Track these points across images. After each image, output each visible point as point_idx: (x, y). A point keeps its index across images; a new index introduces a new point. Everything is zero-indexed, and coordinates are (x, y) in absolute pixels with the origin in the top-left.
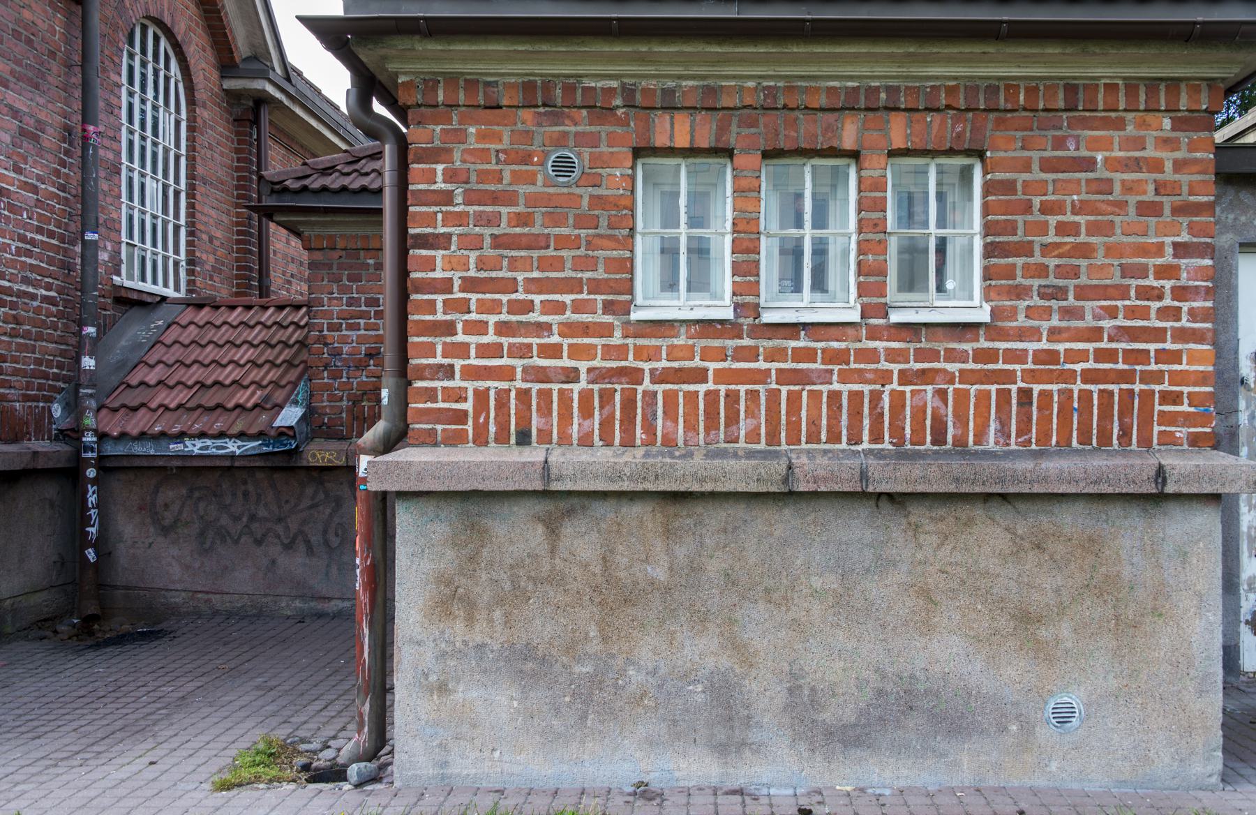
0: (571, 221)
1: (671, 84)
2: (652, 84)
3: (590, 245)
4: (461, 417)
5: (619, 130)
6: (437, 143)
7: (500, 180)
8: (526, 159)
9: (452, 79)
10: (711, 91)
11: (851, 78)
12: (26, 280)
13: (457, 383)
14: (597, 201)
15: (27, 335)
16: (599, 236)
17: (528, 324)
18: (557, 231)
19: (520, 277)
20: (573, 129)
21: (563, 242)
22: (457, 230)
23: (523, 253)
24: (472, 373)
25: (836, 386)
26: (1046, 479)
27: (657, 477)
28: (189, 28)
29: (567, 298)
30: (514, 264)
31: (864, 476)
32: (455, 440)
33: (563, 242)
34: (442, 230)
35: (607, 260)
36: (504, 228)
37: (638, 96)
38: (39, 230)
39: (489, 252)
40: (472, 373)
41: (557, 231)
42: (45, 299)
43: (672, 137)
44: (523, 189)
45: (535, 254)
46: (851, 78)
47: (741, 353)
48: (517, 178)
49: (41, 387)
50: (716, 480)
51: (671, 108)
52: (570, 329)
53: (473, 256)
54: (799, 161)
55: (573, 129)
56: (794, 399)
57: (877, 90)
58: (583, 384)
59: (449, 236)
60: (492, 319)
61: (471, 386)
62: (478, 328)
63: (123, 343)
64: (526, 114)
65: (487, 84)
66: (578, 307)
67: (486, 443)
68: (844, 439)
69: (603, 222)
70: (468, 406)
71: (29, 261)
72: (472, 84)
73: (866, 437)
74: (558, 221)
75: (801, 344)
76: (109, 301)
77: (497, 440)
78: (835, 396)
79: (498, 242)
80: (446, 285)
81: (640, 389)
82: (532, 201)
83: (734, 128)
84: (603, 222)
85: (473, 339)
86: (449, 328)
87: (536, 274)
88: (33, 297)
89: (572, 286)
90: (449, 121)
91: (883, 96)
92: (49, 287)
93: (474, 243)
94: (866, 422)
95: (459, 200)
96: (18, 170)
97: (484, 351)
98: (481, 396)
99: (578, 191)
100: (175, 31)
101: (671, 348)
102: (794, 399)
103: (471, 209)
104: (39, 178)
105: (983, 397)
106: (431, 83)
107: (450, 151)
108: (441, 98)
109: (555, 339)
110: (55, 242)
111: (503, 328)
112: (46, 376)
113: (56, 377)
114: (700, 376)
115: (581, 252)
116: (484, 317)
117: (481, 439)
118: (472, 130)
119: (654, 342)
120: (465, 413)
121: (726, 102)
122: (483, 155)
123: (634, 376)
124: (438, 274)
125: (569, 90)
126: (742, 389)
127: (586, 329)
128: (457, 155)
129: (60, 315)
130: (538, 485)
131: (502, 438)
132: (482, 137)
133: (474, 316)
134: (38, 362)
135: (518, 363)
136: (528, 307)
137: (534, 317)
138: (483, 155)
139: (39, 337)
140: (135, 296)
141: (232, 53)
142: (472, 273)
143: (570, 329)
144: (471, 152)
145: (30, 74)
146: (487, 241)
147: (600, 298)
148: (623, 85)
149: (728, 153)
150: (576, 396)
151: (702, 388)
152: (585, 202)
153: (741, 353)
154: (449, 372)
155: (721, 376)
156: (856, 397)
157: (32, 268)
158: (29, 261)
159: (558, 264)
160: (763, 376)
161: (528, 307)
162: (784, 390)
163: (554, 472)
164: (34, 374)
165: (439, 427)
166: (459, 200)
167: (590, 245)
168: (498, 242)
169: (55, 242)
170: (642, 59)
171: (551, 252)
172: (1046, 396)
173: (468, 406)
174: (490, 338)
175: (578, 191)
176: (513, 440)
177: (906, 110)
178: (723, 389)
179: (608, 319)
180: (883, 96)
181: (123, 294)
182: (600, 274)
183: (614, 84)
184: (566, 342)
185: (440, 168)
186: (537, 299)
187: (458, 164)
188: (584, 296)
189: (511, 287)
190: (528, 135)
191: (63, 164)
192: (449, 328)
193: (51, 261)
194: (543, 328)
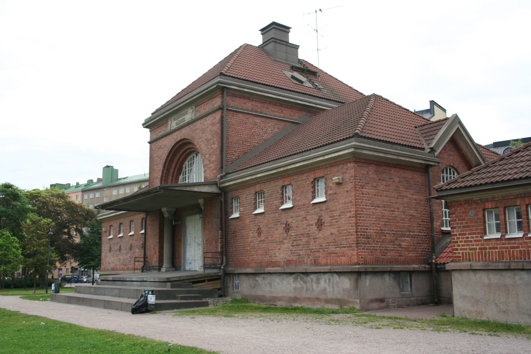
0: (474, 222)
1: (487, 197)
2: (484, 198)
3: (477, 226)
4: (460, 257)
5: (480, 206)
6: (454, 212)
7: (463, 217)
8: (466, 213)
9: (454, 201)
10: (494, 198)
11: (517, 193)
12: (419, 232)
13: (459, 251)
14: (478, 219)
15: (420, 243)
16: (479, 225)
17: (469, 240)
18: (472, 224)
19: (467, 233)
20: (473, 207)
21: (473, 226)
22: (457, 226)
23: (467, 229)
24: (461, 249)
25: (520, 249)
26: (147, 250)
27: (488, 266)
28: (459, 164)
29: (474, 236)
30: (466, 231)
31: (523, 266)
32: (459, 261)
33: (473, 226)
34: (455, 226)
35: (480, 229)
36: (464, 225)
37: (482, 200)
38: (422, 222)
39: (462, 229)
40: (461, 249)
41: (472, 224)
42: (424, 235)
43: (488, 206)
44: (466, 218)
45: (469, 228)
46: (517, 193)
47: (503, 244)
48: (466, 216)
49: (424, 254)
50: (497, 267)
51: (487, 201)
52: (475, 241)
53: (460, 229)
54: (513, 207)
55: (473, 207)
56: (513, 252)
57: (522, 194)
58: (478, 250)
59: (456, 227)
60: (463, 240)
61: (461, 252)
62: (461, 242)
63: (445, 243)
64: (466, 205)
65: (460, 201)
66: (476, 237)
67: (464, 261)
68: (523, 259)
69: (479, 222)
70: (461, 255)
71: (420, 228)
72: (457, 201)
73: (527, 259)
74: (471, 222)
75: (513, 241)
76: (440, 233)
77: (466, 261)
78: (520, 251)
79: (463, 227)
80: (456, 235)
81: (487, 251)
82: (468, 219)
83: (498, 204)
84: (479, 222)
85: (461, 244)
86: (457, 242)
87: (469, 232)
88: (421, 235)
89: (475, 234)
90: (455, 208)
91: (523, 195)
92: (425, 233)
93: (459, 227)
94: (527, 256)
95: (457, 220)
96: (416, 211)
97: (463, 245)
98: (463, 253)
99: (475, 217)
100: (454, 166)
101: (491, 243)
102: (513, 252)
103: (459, 222)
104: (421, 211)
105: (472, 253)
106: (452, 202)
107: (455, 213)
108: (453, 204)
109: (473, 243)
110: (425, 223)
111: (465, 242)
112: (425, 251)
113: (427, 251)
114: (497, 248)
115: (476, 228)
116: (462, 240)
117: (463, 261)
118: (458, 209)
119: (489, 243)
120: (460, 256)
121: (496, 199)
122: (460, 213)
123: (486, 249)
124: (455, 233)
125: (472, 200)
126: (504, 250)
127: (478, 241)
128: (456, 213)
129: (428, 238)
130: (470, 268)
131: (466, 260)
132: (460, 210)
133: (460, 240)
134: (423, 248)
135: (468, 247)
136: (468, 238)
137: (470, 239)
138: (460, 213)
139: (423, 243)
140: (447, 232)
141: (471, 165)
142: (460, 233)
143: (475, 241)
144: (458, 212)
145: (418, 191)
146: (462, 227)
147: (479, 235)
148: (480, 199)
149: (498, 208)
150: (477, 252)
151: (497, 250)
152: (476, 219)
153: (503, 244)
154: (457, 249)
155: (500, 248)
156: (524, 251)
157: (421, 229)
158: (420, 228)
159: (472, 230)
160: (507, 248)
161: (468, 238)
162: (511, 250)
163: (472, 266)
164: (422, 251)
165: (457, 259)
166: (457, 220)
167: (477, 226)
168: (463, 227)
169: (425, 223)
170: (481, 195)
171: (471, 228)
172: (496, 252)
173: (461, 255)
174: (463, 243)
175: (475, 217)
176: (468, 260)
177: (528, 197)
178: (500, 250)
179: (481, 239)
180: (523, 195)
181: (444, 231)
182: (479, 231)
183: (478, 199)
184: (475, 243)
185: (454, 215)
186: (470, 236)
187: (457, 215)
188: (477, 235)
189: (465, 234)
190: (466, 209)
191: (426, 207)
192: (457, 242)
193: (425, 227)
194: (471, 241)
